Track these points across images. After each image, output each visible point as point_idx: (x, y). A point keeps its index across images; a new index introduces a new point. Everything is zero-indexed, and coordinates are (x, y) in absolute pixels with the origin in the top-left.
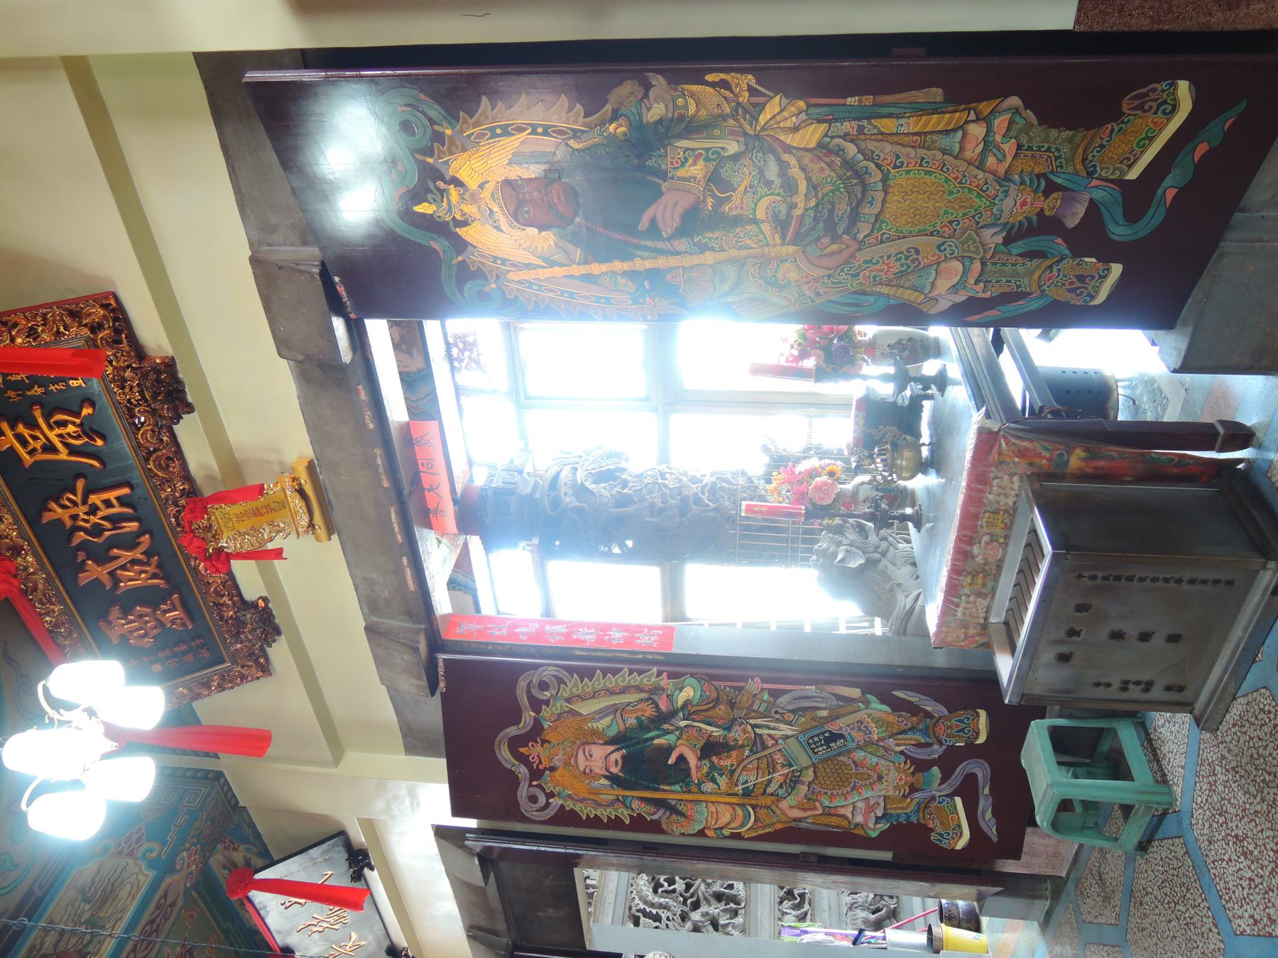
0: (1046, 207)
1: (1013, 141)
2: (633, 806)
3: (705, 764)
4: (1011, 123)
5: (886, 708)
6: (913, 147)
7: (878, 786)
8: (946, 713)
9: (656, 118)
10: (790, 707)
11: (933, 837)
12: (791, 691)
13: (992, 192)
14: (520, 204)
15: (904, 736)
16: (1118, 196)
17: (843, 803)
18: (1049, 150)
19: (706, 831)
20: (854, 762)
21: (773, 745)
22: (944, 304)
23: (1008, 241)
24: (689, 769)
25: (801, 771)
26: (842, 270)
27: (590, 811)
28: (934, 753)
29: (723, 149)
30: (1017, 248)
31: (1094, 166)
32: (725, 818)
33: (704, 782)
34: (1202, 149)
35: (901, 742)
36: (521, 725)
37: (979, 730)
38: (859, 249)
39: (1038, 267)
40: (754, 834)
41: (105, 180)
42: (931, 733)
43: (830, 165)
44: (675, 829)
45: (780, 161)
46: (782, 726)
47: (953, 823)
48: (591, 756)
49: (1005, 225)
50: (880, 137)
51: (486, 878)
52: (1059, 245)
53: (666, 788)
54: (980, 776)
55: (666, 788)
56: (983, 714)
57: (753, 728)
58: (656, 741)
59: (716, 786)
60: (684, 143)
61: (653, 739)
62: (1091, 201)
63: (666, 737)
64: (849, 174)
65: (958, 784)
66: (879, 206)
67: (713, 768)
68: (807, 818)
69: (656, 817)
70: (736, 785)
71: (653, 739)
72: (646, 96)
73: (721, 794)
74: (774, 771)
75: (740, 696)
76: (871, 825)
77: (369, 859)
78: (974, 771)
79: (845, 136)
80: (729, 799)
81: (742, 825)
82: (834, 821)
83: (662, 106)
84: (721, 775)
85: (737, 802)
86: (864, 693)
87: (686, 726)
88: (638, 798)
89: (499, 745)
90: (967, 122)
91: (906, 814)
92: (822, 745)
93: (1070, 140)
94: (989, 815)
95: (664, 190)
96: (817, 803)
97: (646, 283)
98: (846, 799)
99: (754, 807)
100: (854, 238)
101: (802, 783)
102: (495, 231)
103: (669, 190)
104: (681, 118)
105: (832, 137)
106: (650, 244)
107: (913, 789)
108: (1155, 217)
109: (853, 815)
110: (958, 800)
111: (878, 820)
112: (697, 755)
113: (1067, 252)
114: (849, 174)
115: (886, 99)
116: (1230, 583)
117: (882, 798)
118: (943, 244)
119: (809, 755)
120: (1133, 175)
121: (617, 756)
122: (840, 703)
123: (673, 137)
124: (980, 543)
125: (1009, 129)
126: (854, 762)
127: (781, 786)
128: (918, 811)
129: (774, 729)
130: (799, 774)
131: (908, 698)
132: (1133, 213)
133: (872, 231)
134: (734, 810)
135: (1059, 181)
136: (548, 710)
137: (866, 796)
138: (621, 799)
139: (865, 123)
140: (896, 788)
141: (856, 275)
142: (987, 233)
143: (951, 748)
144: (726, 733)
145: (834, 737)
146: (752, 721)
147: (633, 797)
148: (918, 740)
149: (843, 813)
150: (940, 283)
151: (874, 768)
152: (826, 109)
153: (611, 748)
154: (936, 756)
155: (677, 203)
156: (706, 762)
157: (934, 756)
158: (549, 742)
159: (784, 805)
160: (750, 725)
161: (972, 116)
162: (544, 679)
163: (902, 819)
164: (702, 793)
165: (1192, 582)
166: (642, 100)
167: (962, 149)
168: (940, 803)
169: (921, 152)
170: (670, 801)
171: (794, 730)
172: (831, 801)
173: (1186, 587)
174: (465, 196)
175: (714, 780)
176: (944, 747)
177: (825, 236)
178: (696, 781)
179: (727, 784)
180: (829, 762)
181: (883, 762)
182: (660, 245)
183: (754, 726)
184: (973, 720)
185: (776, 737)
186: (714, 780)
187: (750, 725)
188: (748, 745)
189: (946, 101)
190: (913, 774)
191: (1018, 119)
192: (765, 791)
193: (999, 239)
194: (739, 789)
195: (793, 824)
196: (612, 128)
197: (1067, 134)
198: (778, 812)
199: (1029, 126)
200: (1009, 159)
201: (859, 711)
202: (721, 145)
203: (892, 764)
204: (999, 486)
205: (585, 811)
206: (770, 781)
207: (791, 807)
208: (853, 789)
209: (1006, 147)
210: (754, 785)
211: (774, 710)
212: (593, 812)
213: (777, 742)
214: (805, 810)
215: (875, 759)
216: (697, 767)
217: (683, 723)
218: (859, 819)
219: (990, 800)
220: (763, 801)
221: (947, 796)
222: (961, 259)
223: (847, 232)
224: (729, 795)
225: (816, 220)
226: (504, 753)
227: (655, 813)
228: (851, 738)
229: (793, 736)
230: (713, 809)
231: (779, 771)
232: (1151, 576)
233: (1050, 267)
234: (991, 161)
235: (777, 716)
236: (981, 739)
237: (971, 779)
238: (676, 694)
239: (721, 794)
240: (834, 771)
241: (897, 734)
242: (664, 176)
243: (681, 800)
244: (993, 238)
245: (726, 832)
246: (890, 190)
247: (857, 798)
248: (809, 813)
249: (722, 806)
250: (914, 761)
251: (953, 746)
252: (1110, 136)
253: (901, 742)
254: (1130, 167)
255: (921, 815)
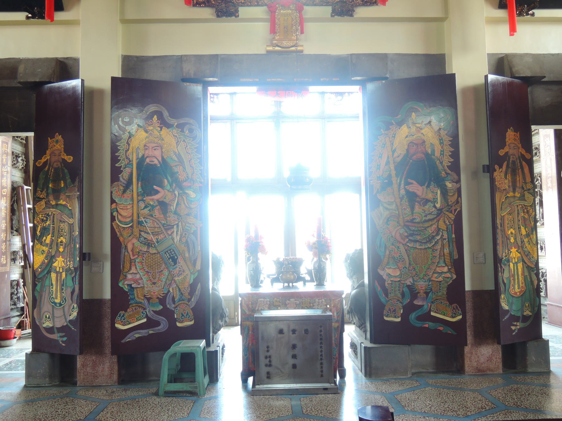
0: (420, 294)
1: (442, 279)
2: (127, 168)
3: (155, 203)
4: (448, 278)
5: (191, 281)
6: (440, 254)
7: (149, 283)
8: (191, 307)
9: (447, 185)
10: (189, 240)
11: (122, 313)
12: (197, 240)
13: (425, 278)
14: (417, 145)
15: (178, 291)
16: (425, 312)
17: (138, 268)
18: (440, 289)
19: (114, 204)
20: (162, 271)
21: (168, 234)
22: (381, 273)
23: (408, 286)
24: (152, 196)
25: (155, 247)
26: (394, 240)
27: (122, 147)
28: (170, 305)
29: (437, 203)
30: (406, 290)
31: (435, 303)
32: (124, 213)
33: (144, 202)
34: (441, 328)
35: (175, 291)
36: (169, 118)
37: (184, 322)
38: (403, 244)
39: (398, 297)
40: (115, 227)
41: (413, 16)
42: (180, 302)
43: (433, 232)
44: (115, 188)
45: (433, 219)
46: (178, 237)
47: (131, 320)
48: (155, 150)
49: (414, 284)
50: (442, 245)
51: (20, 83)
52: (406, 301)
53: (139, 184)
54: (159, 328)
55: (139, 184)
56: (192, 323)
57: (176, 224)
58: (166, 180)
59: (142, 208)
60: (439, 192)
61: (167, 179)
62: (423, 305)
63: (168, 185)
64: (430, 238)
65: (154, 319)
66: (420, 248)
67: (153, 207)
68: (128, 252)
69: (121, 179)
70: (144, 218)
71: (167, 179)
72: (454, 182)
73: (138, 210)
74: (153, 235)
75: (193, 218)
76: (126, 283)
77: (37, 19)
78: (162, 324)
79: (442, 235)
80: (135, 215)
81: (120, 221)
82: (127, 265)
83: (451, 186)
84: (149, 210)
85: (134, 218)
86: (198, 271)
87: (175, 194)
88: (132, 171)
89: (157, 106)
90: (448, 266)
91: (135, 298)
92: (170, 255)
93: (443, 294)
94: (137, 336)
95: (423, 187)
96: (137, 256)
97: (387, 181)
98: (141, 269)
99: (132, 227)
100: (407, 242)
101: (148, 248)
102: (406, 136)
103: (423, 189)
104: (447, 192)
105: (442, 232)
106: (403, 182)
107: (149, 299)
108: (418, 324)
109: (132, 273)
110: (145, 320)
111: (130, 285)
112: (159, 199)
113: (405, 304)
114: (430, 238)
115: (454, 245)
116: (322, 376)
117: (143, 286)
118: (406, 268)
119: (164, 250)
120: (433, 314)
121: (156, 162)
122: (193, 261)
123: (441, 189)
124: (295, 300)
125: (446, 277)
126: (162, 271)
127: (145, 238)
128: (136, 303)
129: (177, 234)
130: (153, 246)
131: (197, 290)
132: (419, 318)
133: (410, 247)
134: (129, 217)
135: (430, 295)
136: (179, 132)
137: (143, 278)
138: (131, 162)
139: (447, 240)
140: (149, 291)
141: (393, 244)
142: (411, 280)
143: (173, 312)
144: (173, 212)
145: (175, 261)
146: (180, 224)
147: (133, 169)
148: (176, 296)
149: (132, 269)
150: (391, 270)
151: (159, 280)
152: (451, 230)
153: (160, 159)
154: (168, 306)
155: (418, 190)
156: (156, 203)
157: (168, 306)
158: (161, 130)
159: (135, 241)
160: (178, 223)
161: (450, 267)
162: (195, 131)
163: (131, 297)
164: (138, 202)
165: (321, 364)
166: (452, 181)
167: (439, 267)
168: (142, 312)
169: (438, 256)
170: (132, 186)
171: (177, 242)
172: (138, 263)
173: (319, 362)
174: (418, 128)
175: (146, 207)
176: (173, 309)
177: (408, 234)
178: (144, 199)
179: (145, 213)
180: (161, 260)
181: (163, 283)
182: (402, 186)
183: (178, 225)
184: (189, 319)
185: (172, 234)
186: (146, 207)
187: (178, 223)
188: (167, 222)
189: (454, 259)
190: (158, 298)
191: (450, 279)
192: (142, 231)
193: (409, 283)
194: (142, 219)
195: (123, 245)
196: (443, 173)
197: (445, 293)
198: (130, 238)
199: (447, 282)
200: (436, 280)
201: (189, 270)
202: (439, 202)
203: (162, 287)
204: (322, 302)
205: (122, 144)
206: (148, 233)
207: (133, 244)
208: (147, 272)
209: (441, 278)
210: (145, 226)
211: (187, 233)
212: (121, 149)
213: (171, 235)
214: (132, 250)
215: (164, 280)
216: (153, 199)
217: (176, 193)
218: (129, 276)
219: (146, 335)
220: (136, 231)
221: (147, 315)
222: (401, 274)
223: (409, 240)
224: (138, 214)
225: (414, 230)
226: (153, 108)
227: (124, 179)
228: (175, 268)
229: (174, 242)
230: (129, 207)
231: (154, 237)
232: (323, 350)
233: (398, 300)
234: (436, 275)
235: (183, 234)
236: (179, 325)
237: (158, 324)
238: (192, 190)
239: (138, 210)
240: (156, 262)
241: (179, 288)
242: (428, 186)
243: (133, 192)
244: (409, 282)
245: (115, 214)
246: (425, 250)
247: (141, 274)
248: (131, 253)
249: (131, 211)
250: (165, 297)
251: (174, 313)
252: (445, 304)
253: (175, 291)
254: (435, 312)
255: (134, 305)
